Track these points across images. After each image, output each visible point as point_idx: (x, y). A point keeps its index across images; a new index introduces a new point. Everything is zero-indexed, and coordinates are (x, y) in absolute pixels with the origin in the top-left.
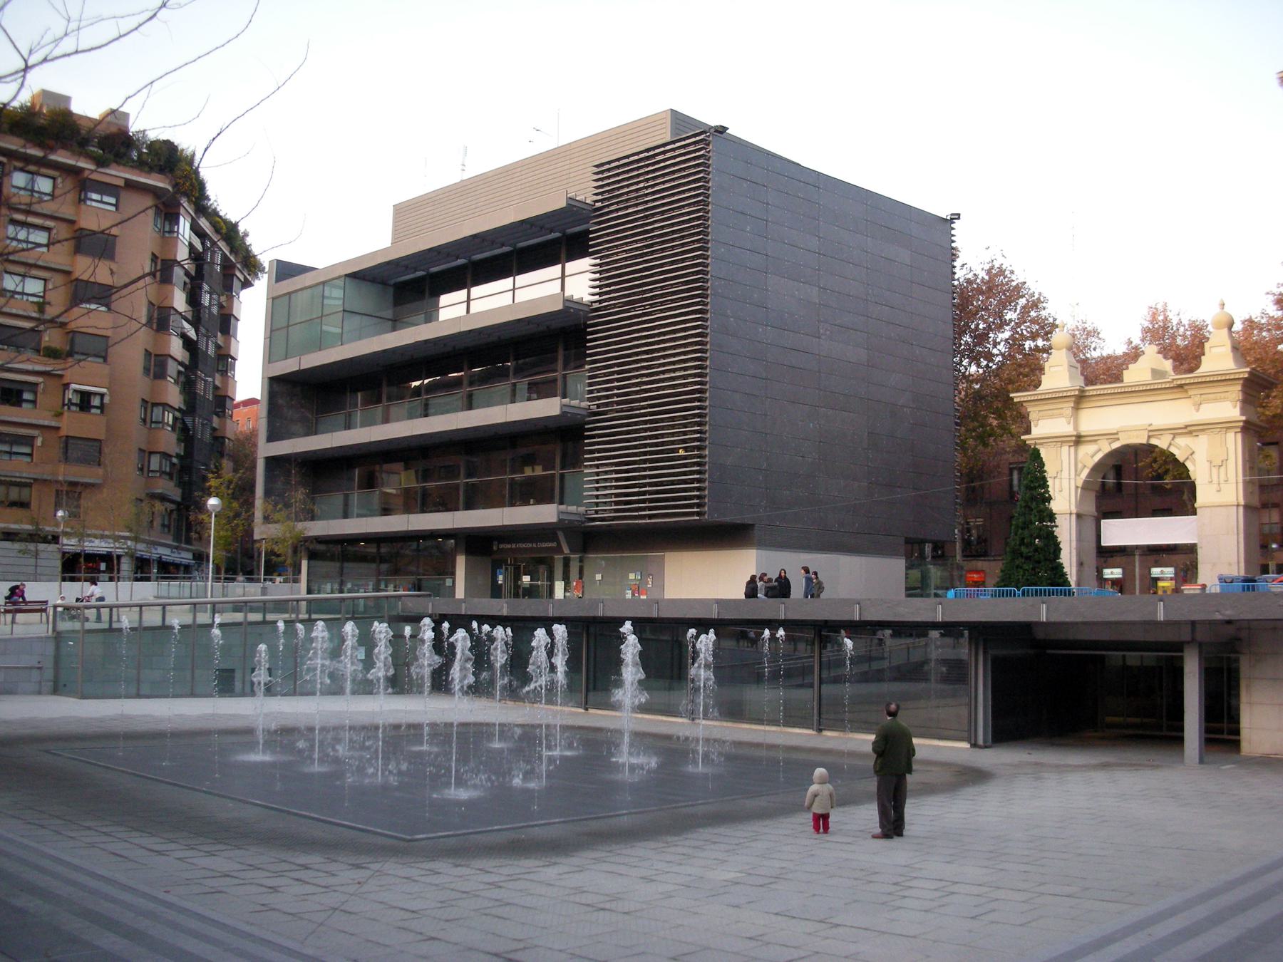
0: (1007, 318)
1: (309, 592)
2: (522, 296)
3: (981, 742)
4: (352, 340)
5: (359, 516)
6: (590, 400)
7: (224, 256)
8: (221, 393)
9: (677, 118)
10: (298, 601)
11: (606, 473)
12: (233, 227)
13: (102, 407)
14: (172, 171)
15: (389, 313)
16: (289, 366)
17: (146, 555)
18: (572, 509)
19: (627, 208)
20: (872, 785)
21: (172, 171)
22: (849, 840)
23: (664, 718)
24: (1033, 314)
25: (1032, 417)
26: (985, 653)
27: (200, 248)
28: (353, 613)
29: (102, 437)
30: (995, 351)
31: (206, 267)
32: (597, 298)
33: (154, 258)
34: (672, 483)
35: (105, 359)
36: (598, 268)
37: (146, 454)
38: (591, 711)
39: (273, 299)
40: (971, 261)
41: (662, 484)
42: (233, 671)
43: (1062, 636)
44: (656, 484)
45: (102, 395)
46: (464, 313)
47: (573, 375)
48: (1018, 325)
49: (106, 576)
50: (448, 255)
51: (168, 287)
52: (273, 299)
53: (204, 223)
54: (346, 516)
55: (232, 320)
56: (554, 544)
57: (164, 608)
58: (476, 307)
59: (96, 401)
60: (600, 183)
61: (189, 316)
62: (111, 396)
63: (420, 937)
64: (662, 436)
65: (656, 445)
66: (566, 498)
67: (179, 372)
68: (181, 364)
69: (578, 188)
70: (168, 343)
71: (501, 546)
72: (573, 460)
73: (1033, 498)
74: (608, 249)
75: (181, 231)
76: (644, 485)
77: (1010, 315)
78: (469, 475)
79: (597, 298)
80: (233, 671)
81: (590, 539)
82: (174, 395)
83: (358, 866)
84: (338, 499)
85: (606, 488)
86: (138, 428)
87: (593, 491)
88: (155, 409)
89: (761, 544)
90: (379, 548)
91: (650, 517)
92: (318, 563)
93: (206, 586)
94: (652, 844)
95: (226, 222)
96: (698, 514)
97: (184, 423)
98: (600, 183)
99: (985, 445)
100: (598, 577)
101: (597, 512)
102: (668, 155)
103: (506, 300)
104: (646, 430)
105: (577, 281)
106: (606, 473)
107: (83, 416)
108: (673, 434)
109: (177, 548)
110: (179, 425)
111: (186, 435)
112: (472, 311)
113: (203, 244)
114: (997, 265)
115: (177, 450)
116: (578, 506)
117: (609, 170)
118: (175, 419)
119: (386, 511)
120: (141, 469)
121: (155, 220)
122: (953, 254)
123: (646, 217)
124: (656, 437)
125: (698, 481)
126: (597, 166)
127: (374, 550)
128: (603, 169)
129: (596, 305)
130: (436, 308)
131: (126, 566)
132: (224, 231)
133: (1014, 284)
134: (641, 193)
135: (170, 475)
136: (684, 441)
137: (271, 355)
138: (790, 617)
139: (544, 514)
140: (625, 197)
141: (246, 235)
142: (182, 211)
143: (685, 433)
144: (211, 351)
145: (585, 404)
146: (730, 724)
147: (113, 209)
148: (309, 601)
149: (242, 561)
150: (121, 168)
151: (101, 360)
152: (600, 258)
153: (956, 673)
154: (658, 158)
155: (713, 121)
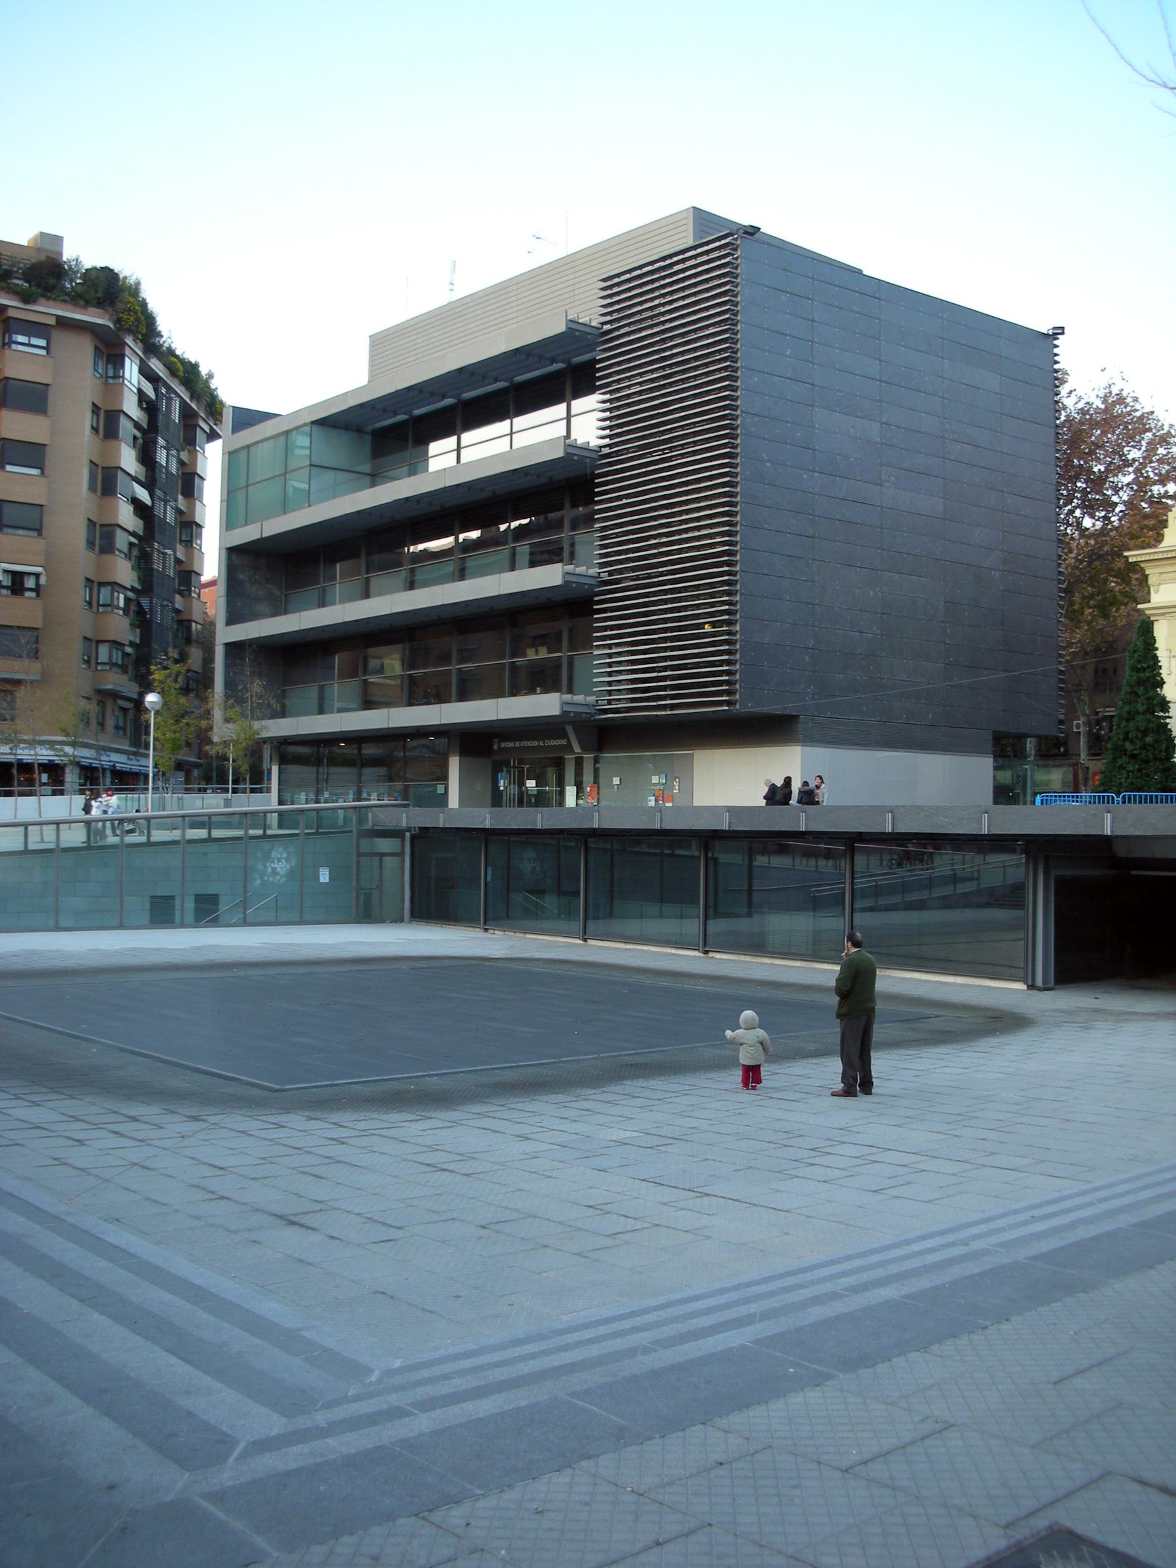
0: (1130, 457)
1: (281, 803)
2: (521, 441)
3: (1039, 982)
4: (320, 501)
5: (340, 711)
6: (602, 565)
7: (183, 403)
8: (185, 568)
9: (702, 218)
10: (265, 813)
11: (620, 654)
12: (193, 368)
13: (37, 589)
14: (112, 303)
15: (367, 468)
16: (248, 534)
17: (95, 763)
18: (579, 698)
19: (640, 330)
20: (833, 1031)
21: (112, 303)
22: (798, 1096)
23: (674, 951)
24: (1161, 451)
25: (1152, 580)
26: (1046, 873)
27: (152, 395)
28: (319, 827)
29: (39, 625)
30: (1115, 499)
31: (160, 417)
32: (607, 441)
33: (96, 409)
34: (697, 665)
35: (39, 531)
36: (608, 405)
37: (92, 643)
38: (590, 942)
39: (230, 453)
40: (1083, 386)
41: (685, 667)
42: (173, 898)
43: (1147, 854)
44: (679, 667)
45: (37, 575)
46: (454, 463)
47: (581, 536)
48: (1143, 465)
49: (49, 789)
50: (432, 394)
51: (112, 443)
52: (230, 453)
53: (156, 365)
54: (321, 711)
55: (197, 479)
56: (564, 742)
57: (26, 829)
58: (467, 456)
59: (30, 583)
60: (609, 301)
61: (143, 479)
62: (47, 574)
63: (209, 1196)
64: (686, 608)
65: (680, 619)
66: (575, 688)
67: (131, 544)
68: (133, 534)
69: (578, 309)
70: (115, 509)
71: (503, 745)
72: (581, 641)
73: (1140, 682)
74: (618, 381)
75: (127, 375)
76: (665, 669)
77: (1134, 454)
78: (463, 660)
79: (607, 441)
80: (173, 898)
81: (607, 735)
82: (125, 572)
83: (196, 1119)
84: (312, 692)
85: (620, 672)
86: (81, 611)
87: (604, 677)
88: (103, 590)
89: (809, 740)
90: (360, 749)
91: (672, 707)
92: (292, 768)
93: (146, 798)
94: (560, 1098)
95: (183, 361)
96: (728, 703)
97: (139, 605)
98: (609, 301)
99: (1106, 616)
100: (616, 781)
101: (609, 702)
102: (688, 264)
103: (502, 446)
104: (666, 602)
105: (584, 422)
106: (620, 654)
107: (17, 600)
108: (698, 606)
109: (134, 754)
110: (133, 608)
111: (141, 619)
112: (463, 461)
113: (156, 390)
114: (1115, 391)
115: (132, 638)
116: (586, 695)
117: (618, 284)
118: (127, 600)
119: (368, 704)
120: (88, 662)
121: (95, 364)
122: (1056, 379)
123: (663, 341)
124: (679, 609)
125: (728, 662)
126: (604, 280)
127: (355, 752)
128: (611, 283)
129: (606, 451)
130: (425, 458)
131: (71, 777)
132: (181, 373)
133: (1138, 414)
134: (656, 311)
135: (123, 668)
136: (712, 615)
137: (229, 521)
138: (902, 828)
139: (543, 705)
140: (638, 317)
141: (211, 376)
142: (127, 351)
143: (712, 605)
144: (170, 517)
145: (593, 571)
146: (748, 958)
147: (43, 352)
148: (281, 814)
149: (203, 769)
150: (52, 303)
151: (35, 534)
152: (610, 392)
153: (1013, 897)
154: (676, 268)
155: (745, 221)
